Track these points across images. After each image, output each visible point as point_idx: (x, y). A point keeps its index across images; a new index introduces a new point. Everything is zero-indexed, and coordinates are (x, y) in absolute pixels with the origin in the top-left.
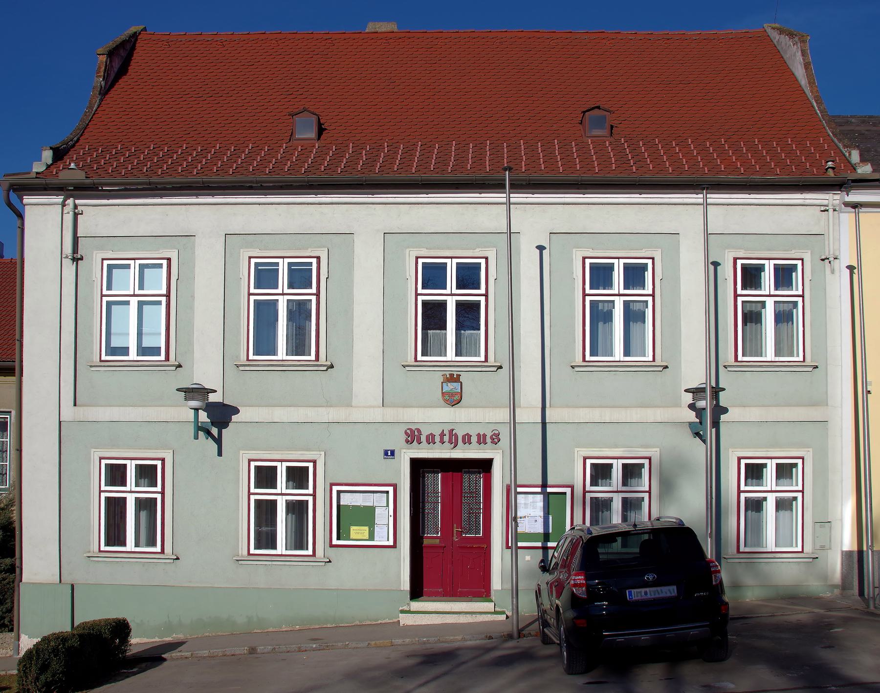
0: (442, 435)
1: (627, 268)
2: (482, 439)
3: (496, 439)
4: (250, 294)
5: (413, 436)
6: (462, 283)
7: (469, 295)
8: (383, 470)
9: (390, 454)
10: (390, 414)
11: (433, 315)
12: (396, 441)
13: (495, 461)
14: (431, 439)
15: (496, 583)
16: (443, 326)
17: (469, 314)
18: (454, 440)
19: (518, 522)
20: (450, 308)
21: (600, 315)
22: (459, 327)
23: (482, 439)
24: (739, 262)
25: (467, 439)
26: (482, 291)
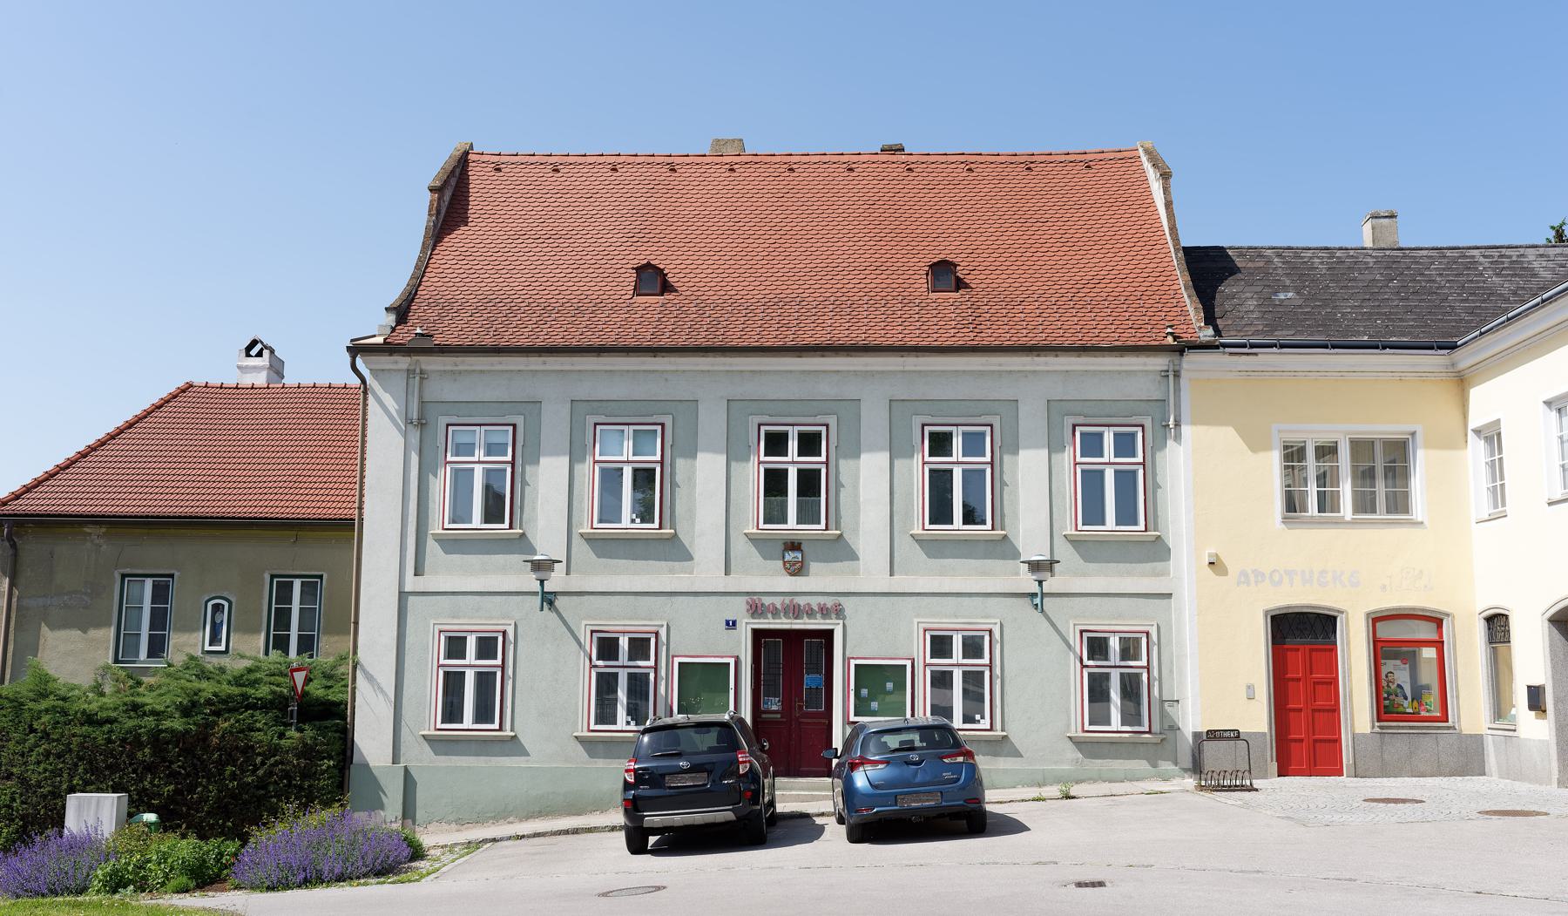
7: (810, 461)
9: (730, 625)
16: (1107, 698)
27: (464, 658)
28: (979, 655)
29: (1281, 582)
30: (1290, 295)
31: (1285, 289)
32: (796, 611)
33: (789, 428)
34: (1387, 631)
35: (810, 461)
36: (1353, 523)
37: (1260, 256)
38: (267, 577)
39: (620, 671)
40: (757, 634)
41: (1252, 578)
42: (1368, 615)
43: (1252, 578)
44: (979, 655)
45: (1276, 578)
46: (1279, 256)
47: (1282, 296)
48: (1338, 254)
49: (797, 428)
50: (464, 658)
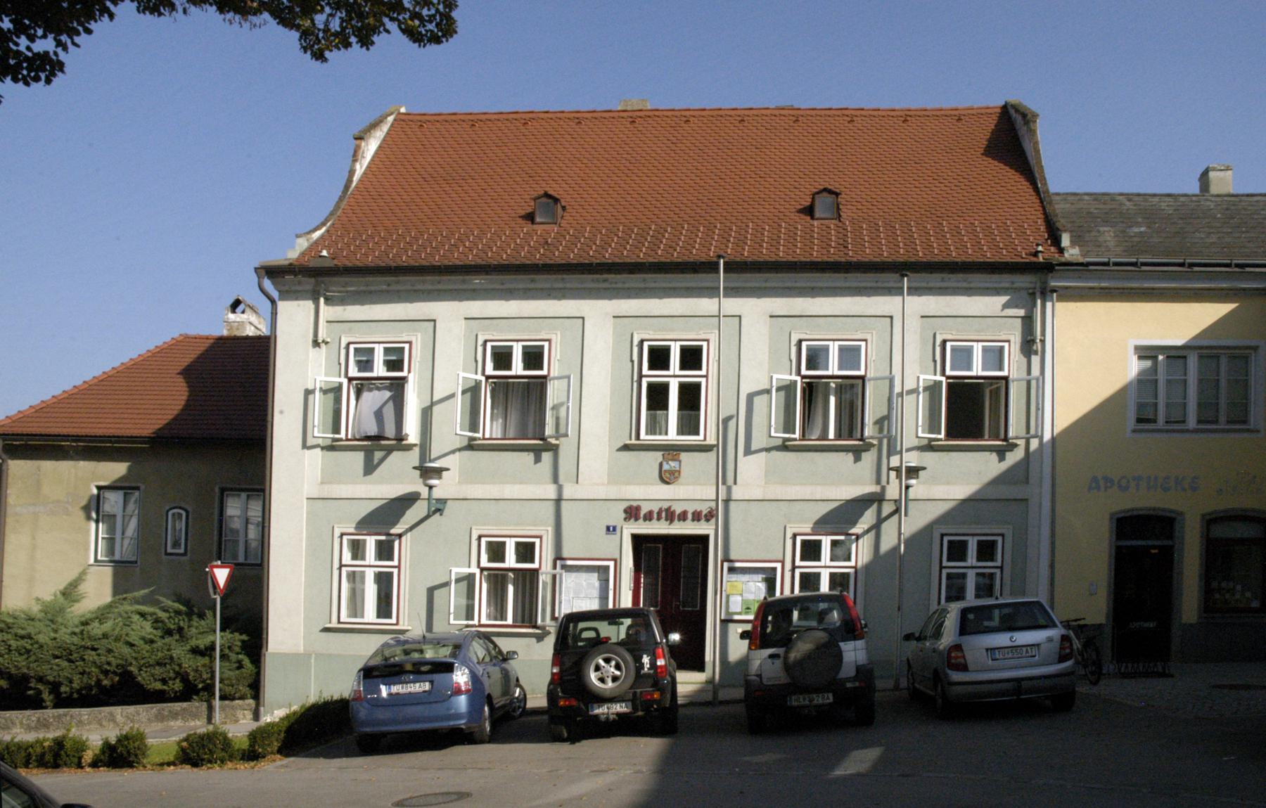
0: (659, 513)
1: (684, 351)
2: (697, 517)
3: (710, 516)
4: (706, 376)
5: (632, 513)
6: (684, 365)
7: (691, 376)
8: (607, 546)
9: (610, 530)
10: (613, 492)
11: (658, 396)
12: (617, 516)
13: (362, 472)
14: (649, 517)
15: (708, 657)
16: (665, 407)
17: (690, 396)
18: (670, 516)
19: (734, 597)
20: (670, 390)
21: (658, 396)
22: (682, 406)
23: (697, 517)
24: (863, 344)
25: (683, 517)
26: (703, 372)
27: (819, 559)
28: (391, 558)
29: (1127, 488)
30: (1143, 229)
31: (1138, 224)
32: (670, 516)
33: (672, 344)
34: (1219, 531)
35: (691, 376)
36: (1196, 431)
37: (1113, 200)
38: (217, 490)
39: (829, 563)
40: (638, 540)
41: (1102, 483)
42: (1203, 516)
43: (1102, 483)
44: (391, 558)
45: (1124, 482)
46: (1129, 200)
47: (1136, 230)
48: (1182, 199)
49: (679, 344)
50: (819, 559)
